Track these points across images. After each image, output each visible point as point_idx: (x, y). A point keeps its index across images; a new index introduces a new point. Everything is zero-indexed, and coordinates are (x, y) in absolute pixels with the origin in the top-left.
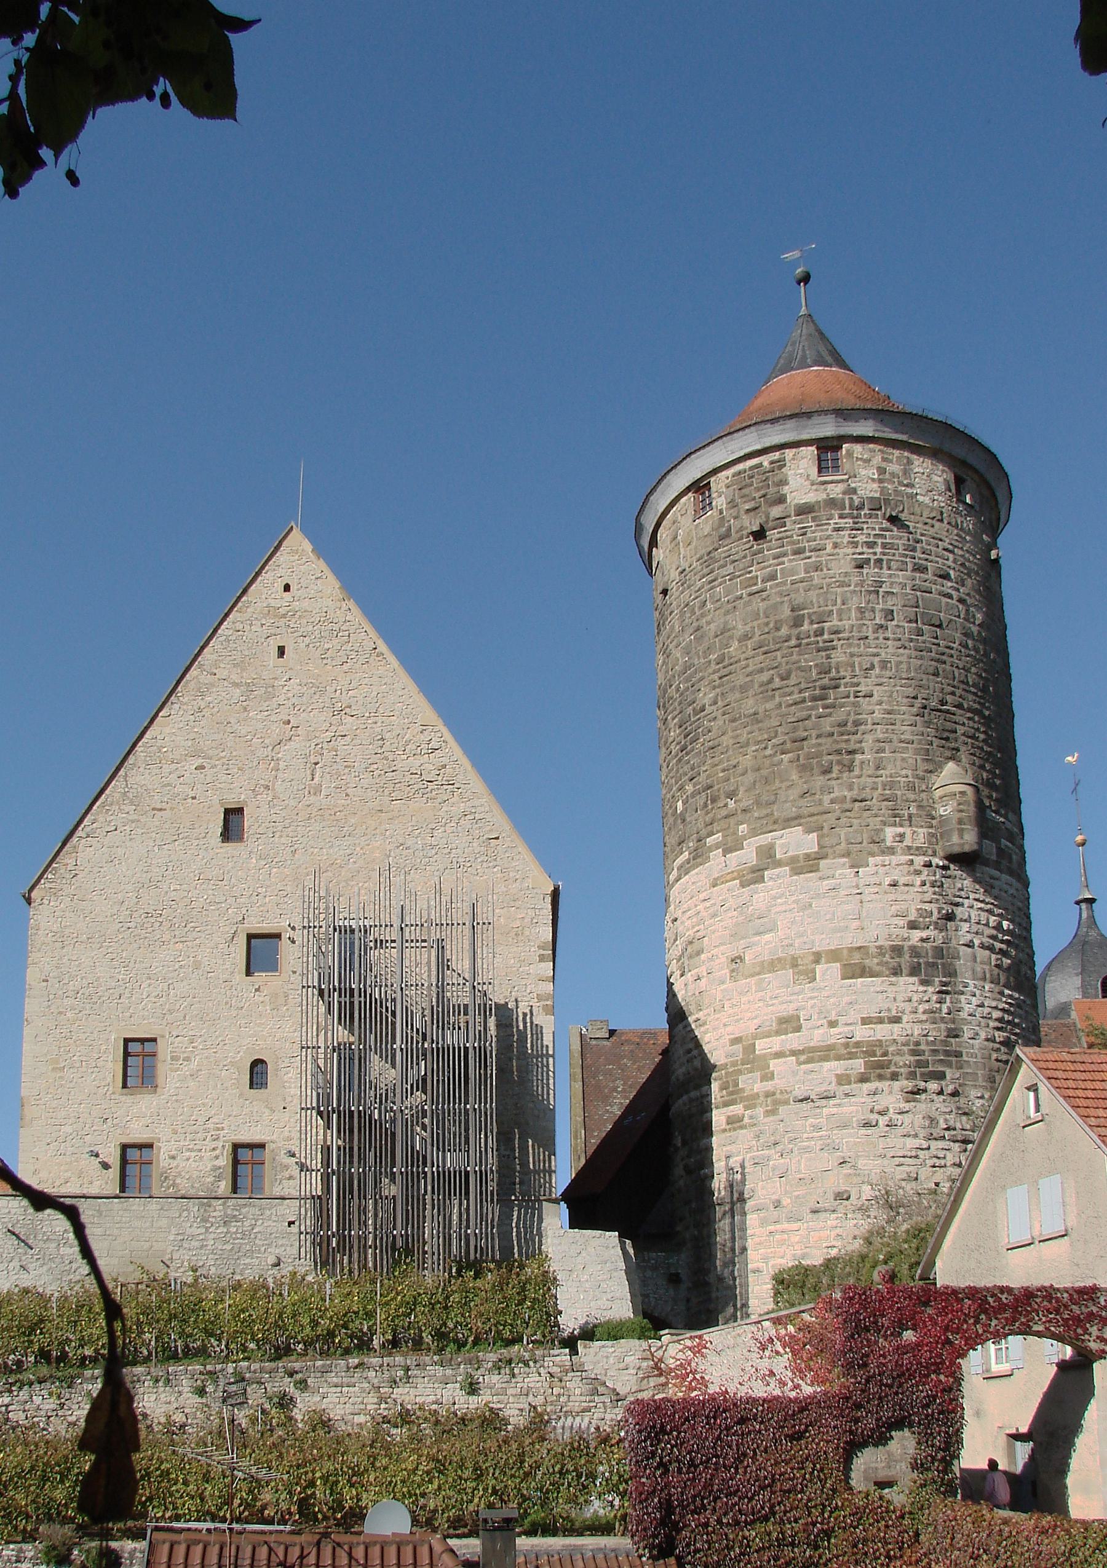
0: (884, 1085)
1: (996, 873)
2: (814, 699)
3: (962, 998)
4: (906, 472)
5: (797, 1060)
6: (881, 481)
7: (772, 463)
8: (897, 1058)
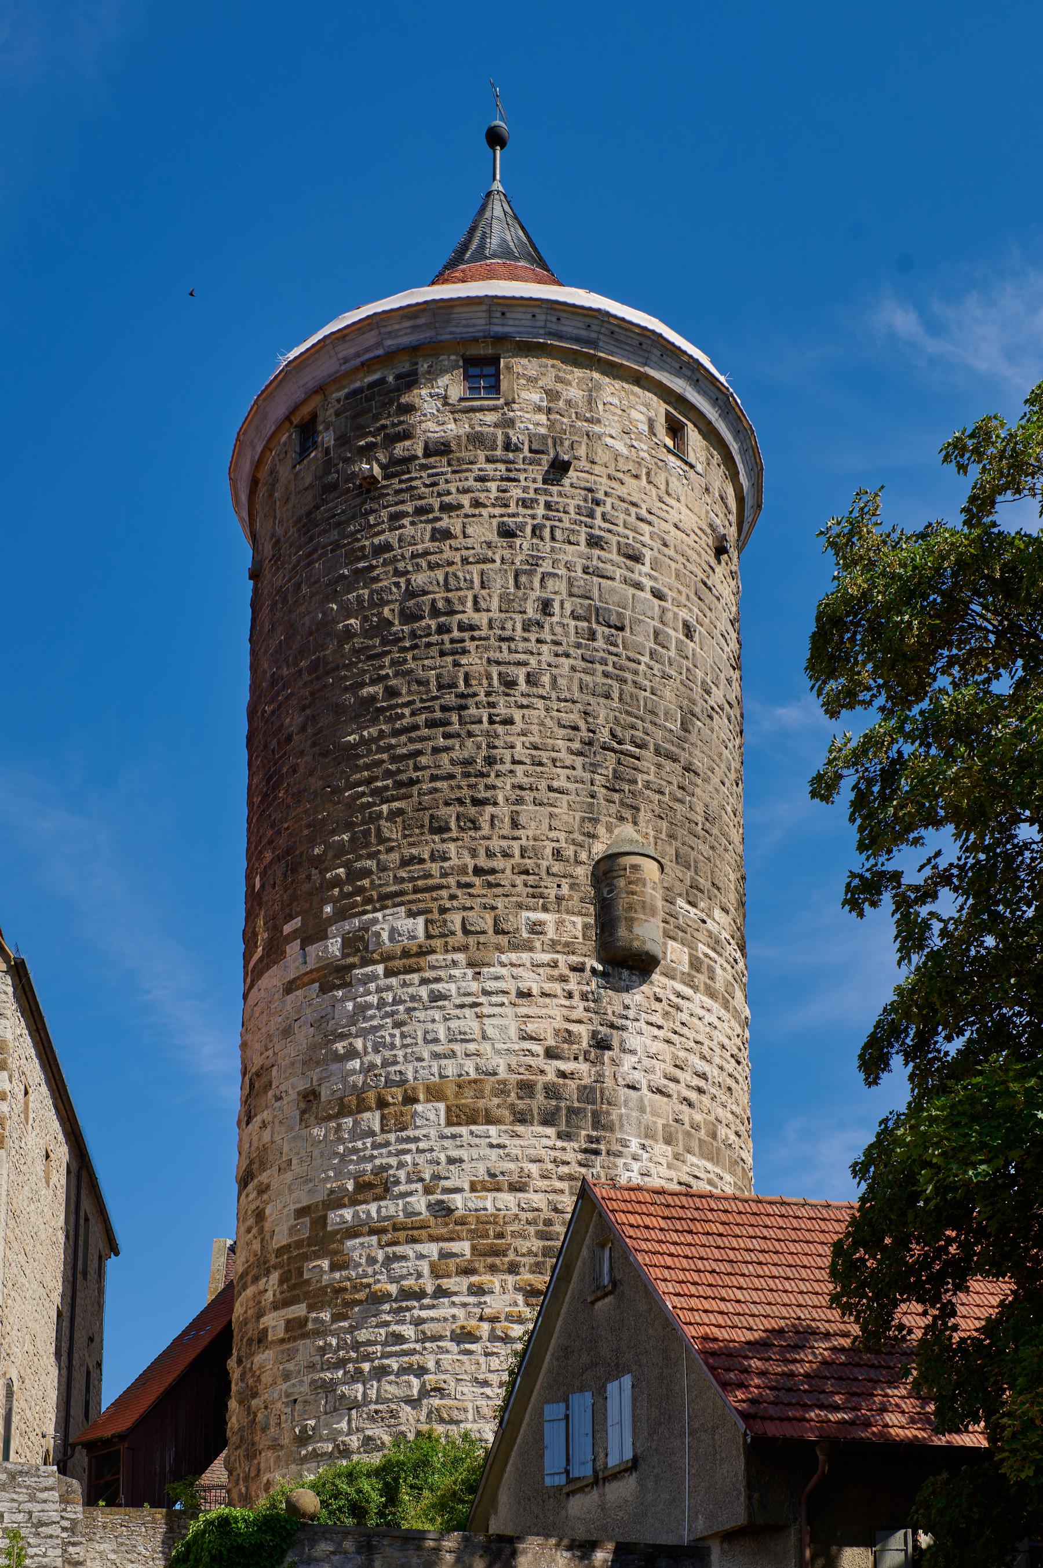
0: (494, 1281)
1: (687, 991)
2: (432, 724)
3: (620, 1162)
4: (590, 401)
6: (549, 411)
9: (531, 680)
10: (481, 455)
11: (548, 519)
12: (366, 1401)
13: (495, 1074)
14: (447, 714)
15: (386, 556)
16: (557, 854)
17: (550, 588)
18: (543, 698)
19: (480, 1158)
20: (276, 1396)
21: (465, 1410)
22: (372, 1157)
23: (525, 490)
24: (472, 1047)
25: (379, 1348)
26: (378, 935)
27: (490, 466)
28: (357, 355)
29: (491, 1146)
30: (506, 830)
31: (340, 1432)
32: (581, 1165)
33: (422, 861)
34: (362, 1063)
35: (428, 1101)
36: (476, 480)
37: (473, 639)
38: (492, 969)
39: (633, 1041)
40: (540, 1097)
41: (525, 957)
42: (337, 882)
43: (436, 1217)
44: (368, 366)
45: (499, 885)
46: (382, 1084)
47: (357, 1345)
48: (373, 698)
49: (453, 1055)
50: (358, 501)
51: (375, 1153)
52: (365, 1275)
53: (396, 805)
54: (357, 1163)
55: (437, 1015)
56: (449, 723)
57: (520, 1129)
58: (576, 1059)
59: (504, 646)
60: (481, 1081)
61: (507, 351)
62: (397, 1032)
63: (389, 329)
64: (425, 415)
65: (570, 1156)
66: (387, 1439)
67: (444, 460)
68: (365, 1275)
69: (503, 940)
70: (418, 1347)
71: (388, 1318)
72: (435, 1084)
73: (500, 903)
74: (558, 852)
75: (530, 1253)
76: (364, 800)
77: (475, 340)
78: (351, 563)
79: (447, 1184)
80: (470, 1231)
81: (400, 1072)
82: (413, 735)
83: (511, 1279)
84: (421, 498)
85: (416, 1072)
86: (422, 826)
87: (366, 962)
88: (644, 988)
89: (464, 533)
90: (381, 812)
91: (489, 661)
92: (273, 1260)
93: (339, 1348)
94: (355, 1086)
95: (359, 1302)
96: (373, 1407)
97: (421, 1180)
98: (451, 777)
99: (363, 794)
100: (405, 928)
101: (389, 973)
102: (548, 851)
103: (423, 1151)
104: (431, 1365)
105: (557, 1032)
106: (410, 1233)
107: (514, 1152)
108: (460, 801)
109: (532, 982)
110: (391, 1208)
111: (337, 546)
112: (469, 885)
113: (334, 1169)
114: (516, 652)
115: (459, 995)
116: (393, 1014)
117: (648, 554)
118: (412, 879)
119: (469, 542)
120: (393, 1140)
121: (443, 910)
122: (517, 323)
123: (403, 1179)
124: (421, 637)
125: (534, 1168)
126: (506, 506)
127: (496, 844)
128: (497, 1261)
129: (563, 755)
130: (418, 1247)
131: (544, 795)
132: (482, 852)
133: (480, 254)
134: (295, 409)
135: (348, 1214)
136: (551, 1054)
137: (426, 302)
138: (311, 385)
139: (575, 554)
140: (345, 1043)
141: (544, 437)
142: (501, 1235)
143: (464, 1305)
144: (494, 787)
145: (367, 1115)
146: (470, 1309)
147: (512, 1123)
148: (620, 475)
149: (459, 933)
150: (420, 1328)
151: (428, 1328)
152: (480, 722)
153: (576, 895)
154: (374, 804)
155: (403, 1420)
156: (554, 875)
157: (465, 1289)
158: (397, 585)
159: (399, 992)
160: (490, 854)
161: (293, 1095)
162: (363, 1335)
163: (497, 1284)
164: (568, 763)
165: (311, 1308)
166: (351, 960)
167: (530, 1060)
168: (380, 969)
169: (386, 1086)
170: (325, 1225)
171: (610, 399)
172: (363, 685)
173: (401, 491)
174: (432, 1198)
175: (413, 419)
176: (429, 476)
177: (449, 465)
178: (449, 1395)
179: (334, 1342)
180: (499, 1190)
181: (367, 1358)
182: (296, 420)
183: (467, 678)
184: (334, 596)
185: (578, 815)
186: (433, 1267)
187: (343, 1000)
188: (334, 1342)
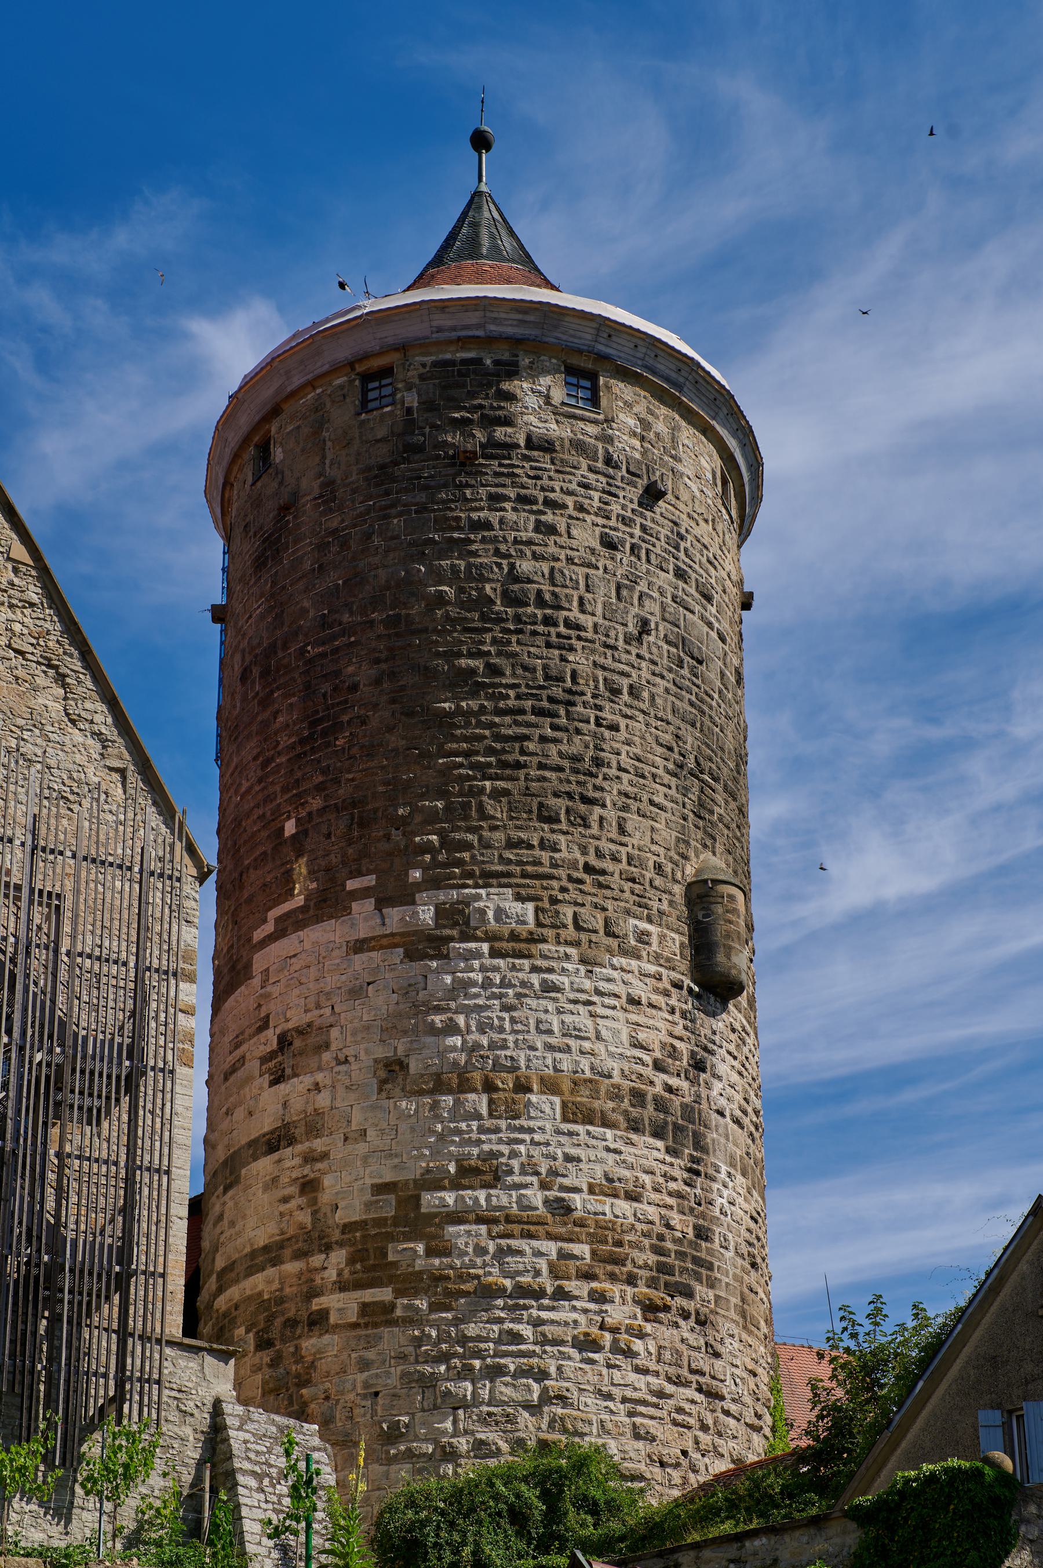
0: (615, 1290)
3: (715, 1186)
5: (489, 1232)
6: (643, 439)
7: (497, 363)
8: (635, 1253)
9: (633, 691)
10: (584, 463)
11: (644, 541)
12: (476, 1401)
13: (610, 1077)
14: (556, 707)
15: (486, 534)
16: (659, 868)
17: (647, 608)
18: (643, 712)
19: (598, 1161)
20: (348, 1386)
21: (590, 1423)
22: (479, 1142)
23: (624, 507)
24: (587, 1045)
26: (482, 912)
27: (591, 476)
28: (454, 329)
29: (608, 1149)
30: (614, 835)
31: (444, 1432)
32: (686, 1184)
33: (530, 847)
34: (464, 1042)
35: (543, 1093)
36: (579, 485)
37: (579, 638)
38: (604, 970)
39: (722, 1069)
40: (651, 1107)
41: (634, 964)
42: (428, 848)
43: (553, 1215)
44: (463, 342)
45: (608, 887)
46: (490, 1067)
47: (463, 1340)
48: (473, 672)
49: (568, 1049)
50: (451, 471)
51: (483, 1137)
53: (501, 784)
54: (460, 1144)
56: (557, 716)
57: (634, 1137)
58: (678, 1075)
59: (609, 653)
60: (596, 1082)
61: (607, 371)
62: (506, 1015)
64: (527, 408)
65: (677, 1173)
66: (504, 1447)
67: (548, 457)
69: (614, 943)
70: (538, 1349)
72: (550, 1077)
73: (609, 905)
74: (660, 867)
75: (646, 1266)
76: (462, 771)
77: (580, 352)
78: (443, 530)
79: (566, 1182)
80: (589, 1234)
81: (512, 1058)
82: (519, 718)
83: (630, 1290)
84: (523, 487)
85: (529, 1060)
86: (530, 812)
87: (465, 938)
88: (724, 1016)
89: (569, 533)
90: (484, 788)
91: (595, 664)
92: (336, 1236)
93: (440, 1340)
94: (455, 1063)
95: (466, 1294)
96: (485, 1409)
97: (537, 1173)
98: (560, 769)
99: (461, 765)
100: (513, 911)
101: (494, 953)
102: (651, 864)
103: (539, 1144)
104: (553, 1370)
105: (663, 1045)
106: (526, 1227)
107: (631, 1159)
108: (570, 796)
109: (641, 990)
110: (502, 1198)
111: (422, 509)
112: (580, 882)
113: (429, 1147)
114: (620, 662)
115: (573, 990)
116: (500, 996)
117: (716, 597)
118: (520, 863)
119: (574, 544)
120: (504, 1127)
121: (554, 901)
123: (516, 1170)
124: (526, 623)
125: (647, 1179)
126: (608, 518)
127: (606, 846)
128: (616, 1269)
129: (660, 772)
130: (535, 1243)
131: (645, 806)
132: (592, 851)
133: (473, 250)
134: (366, 357)
135: (450, 1198)
136: (658, 1066)
137: (540, 303)
138: (390, 341)
139: (665, 579)
140: (443, 1017)
141: (638, 462)
142: (619, 1244)
143: (586, 1311)
144: (602, 789)
145: (471, 1096)
146: (591, 1316)
147: (627, 1129)
148: (696, 516)
149: (571, 927)
150: (539, 1329)
152: (588, 722)
153: (675, 913)
154: (475, 778)
155: (521, 1426)
156: (656, 888)
158: (499, 566)
159: (509, 975)
160: (599, 854)
161: (366, 1060)
162: (472, 1330)
163: (617, 1294)
164: (666, 782)
165: (399, 1293)
166: (447, 932)
167: (639, 1068)
168: (485, 947)
169: (493, 1070)
170: (418, 1206)
171: (686, 442)
172: (459, 655)
173: (502, 474)
174: (552, 1194)
175: (514, 408)
176: (532, 468)
177: (553, 463)
178: (572, 1404)
179: (434, 1334)
180: (616, 1196)
181: (478, 1354)
182: (360, 368)
183: (574, 675)
184: (421, 557)
185: (674, 834)
186: (551, 1266)
187: (438, 972)
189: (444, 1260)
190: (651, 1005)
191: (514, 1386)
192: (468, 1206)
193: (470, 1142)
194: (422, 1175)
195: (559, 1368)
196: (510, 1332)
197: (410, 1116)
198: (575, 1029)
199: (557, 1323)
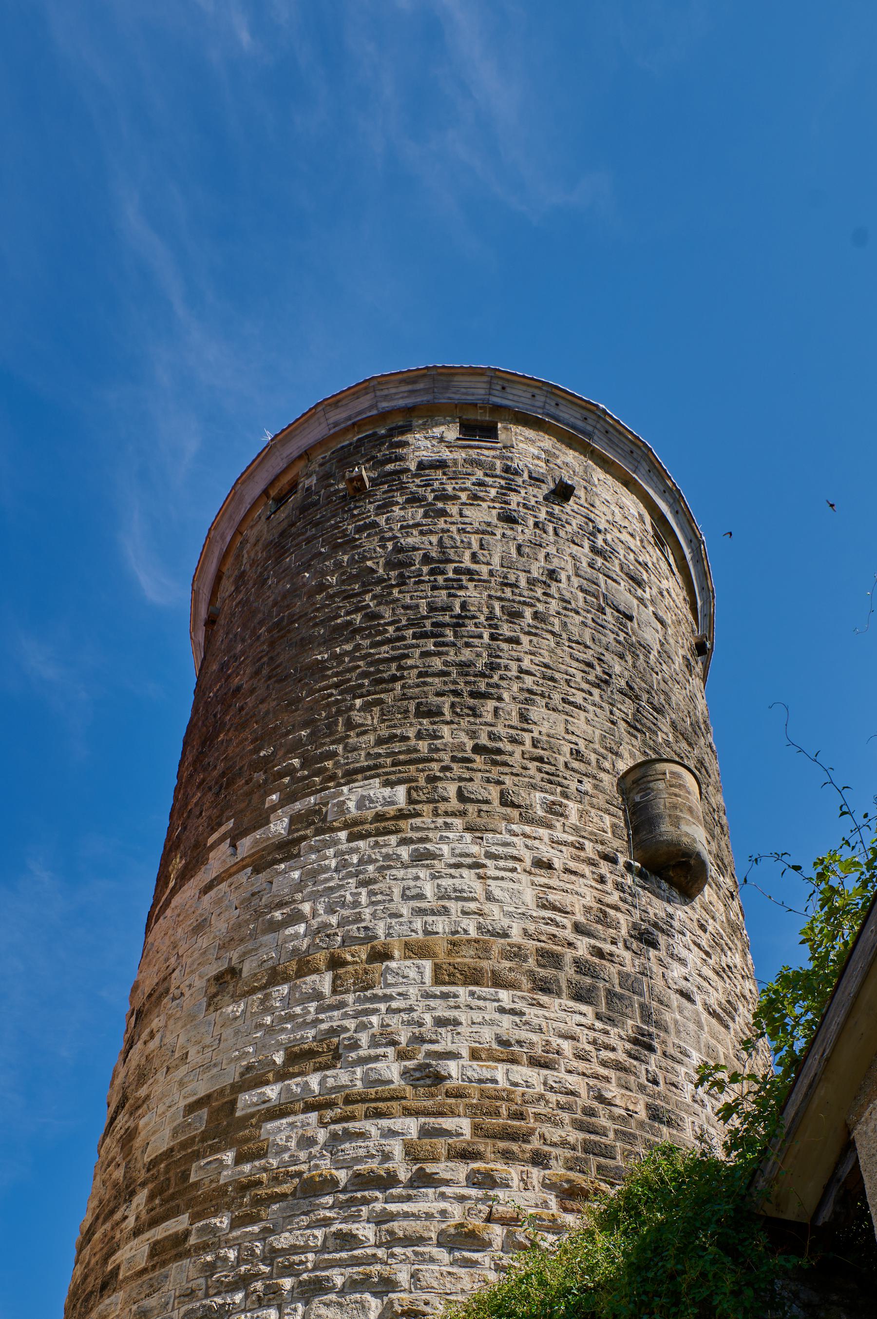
8: (546, 1129)
13: (506, 935)
22: (316, 1022)
25: (311, 1256)
28: (349, 418)
29: (502, 1010)
32: (630, 1055)
35: (406, 958)
43: (415, 1087)
51: (322, 1016)
52: (295, 1161)
55: (423, 873)
57: (544, 999)
59: (508, 590)
60: (485, 942)
62: (364, 891)
63: (385, 392)
65: (613, 1041)
67: (440, 472)
68: (295, 1161)
69: (515, 813)
70: (381, 1253)
71: (329, 1214)
75: (564, 1143)
83: (536, 1174)
93: (239, 1261)
95: (283, 1196)
97: (394, 1043)
103: (399, 1011)
104: (403, 1277)
106: (373, 1105)
118: (388, 755)
119: (467, 520)
122: (516, 398)
125: (567, 1046)
128: (514, 1147)
130: (384, 1123)
138: (296, 454)
142: (520, 1116)
143: (462, 1199)
144: (498, 686)
146: (469, 1204)
150: (385, 1227)
151: (398, 1227)
157: (462, 1177)
162: (283, 1240)
168: (343, 835)
179: (232, 1255)
180: (514, 1061)
181: (289, 1270)
182: (273, 493)
188: (232, 1255)
189: (257, 1163)
190: (567, 871)
191: (340, 1305)
192: (296, 1095)
193: (305, 1025)
194: (242, 1075)
195: (414, 1276)
196: (339, 1235)
197: (236, 1018)
198: (455, 890)
199: (416, 1217)
